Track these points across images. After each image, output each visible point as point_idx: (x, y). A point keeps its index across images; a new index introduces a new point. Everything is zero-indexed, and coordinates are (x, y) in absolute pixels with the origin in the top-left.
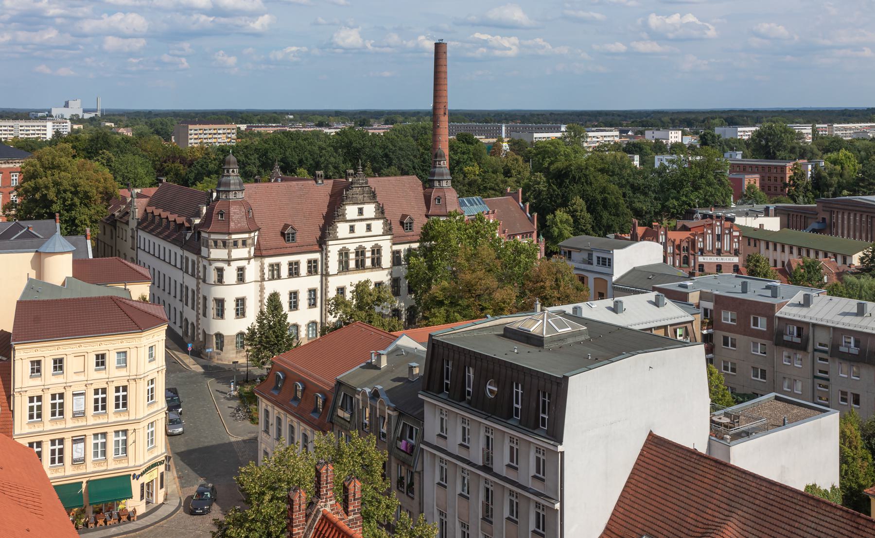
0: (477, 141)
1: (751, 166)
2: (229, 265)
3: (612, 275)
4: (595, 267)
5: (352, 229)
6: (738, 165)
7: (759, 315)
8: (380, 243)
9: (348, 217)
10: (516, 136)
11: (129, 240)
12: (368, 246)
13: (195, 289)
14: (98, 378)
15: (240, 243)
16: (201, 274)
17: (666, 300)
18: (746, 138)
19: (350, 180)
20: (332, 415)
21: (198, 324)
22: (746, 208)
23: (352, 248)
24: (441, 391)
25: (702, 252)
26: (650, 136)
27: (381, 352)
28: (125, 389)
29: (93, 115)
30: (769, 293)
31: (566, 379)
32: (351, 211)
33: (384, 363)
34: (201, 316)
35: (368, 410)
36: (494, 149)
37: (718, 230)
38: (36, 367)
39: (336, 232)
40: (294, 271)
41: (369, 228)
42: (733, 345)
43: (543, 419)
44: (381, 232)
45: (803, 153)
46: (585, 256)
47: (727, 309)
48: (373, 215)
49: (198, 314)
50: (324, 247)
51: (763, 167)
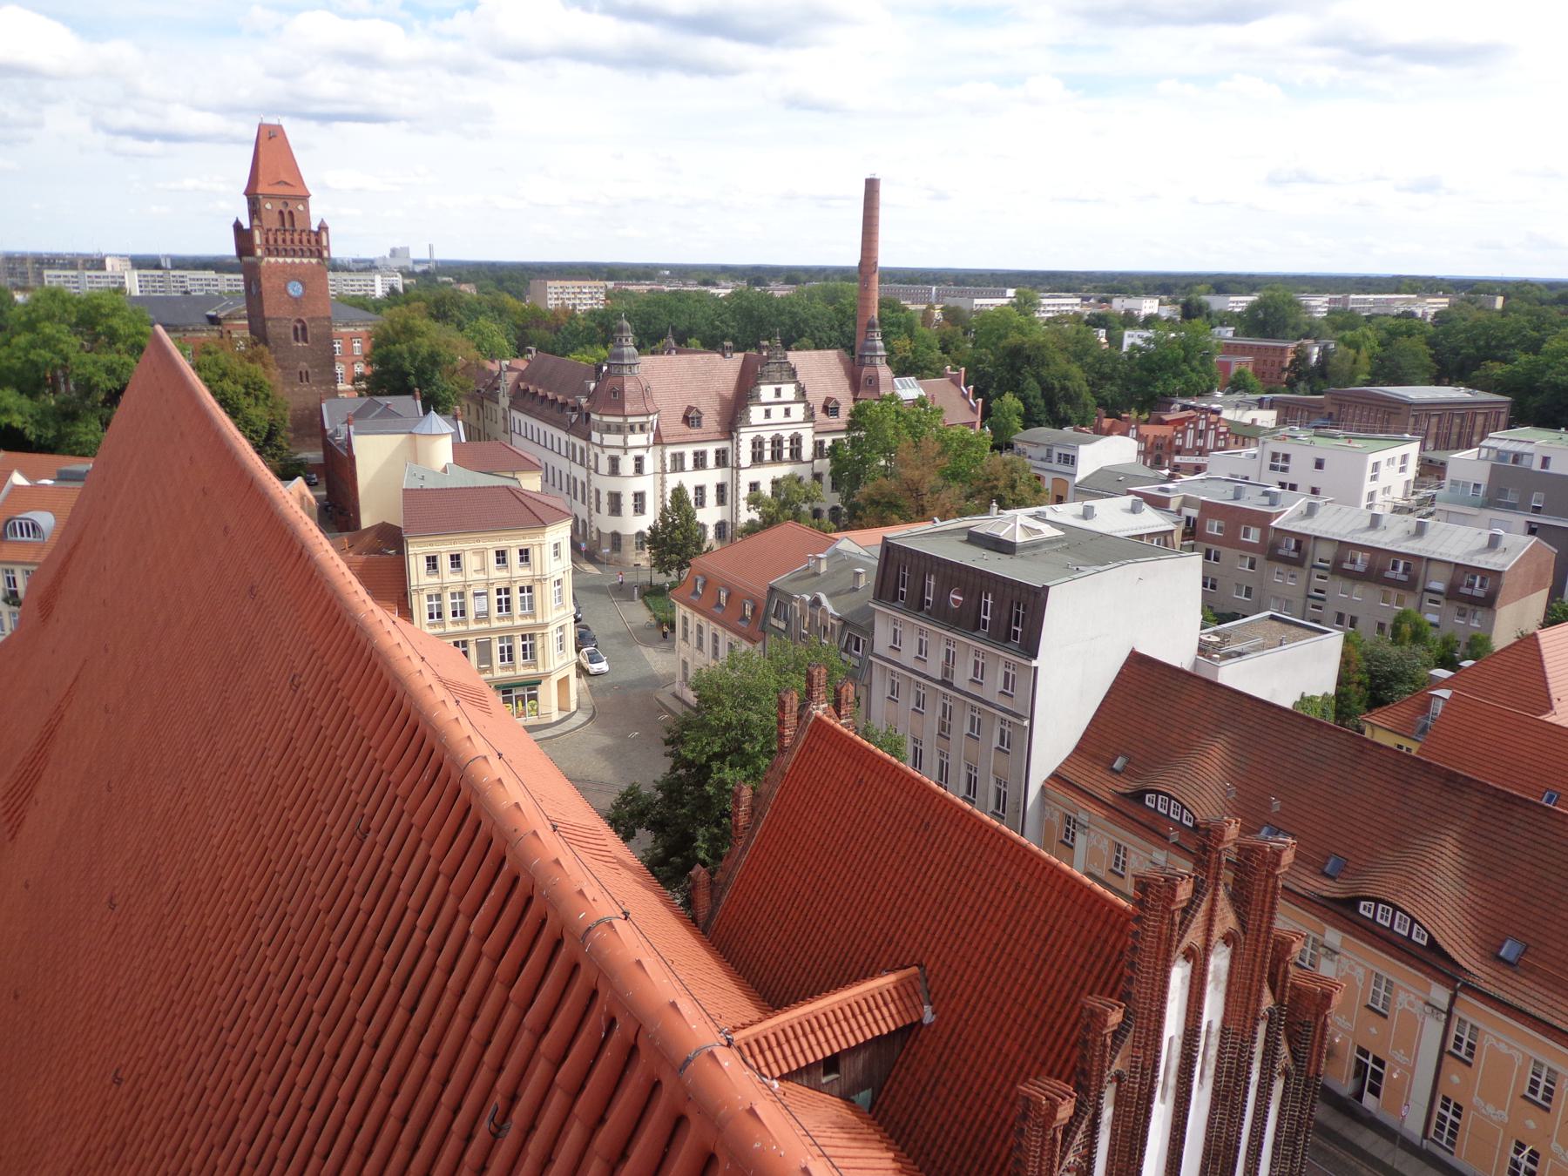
0: (904, 309)
1: (1244, 346)
2: (626, 453)
3: (1074, 475)
4: (1055, 466)
5: (768, 414)
6: (1228, 345)
7: (1253, 525)
8: (799, 431)
9: (764, 399)
10: (951, 302)
11: (501, 421)
12: (786, 435)
13: (585, 480)
14: (497, 575)
15: (637, 427)
16: (592, 464)
17: (1145, 506)
18: (1237, 310)
19: (765, 354)
20: (764, 623)
21: (590, 521)
22: (1237, 397)
23: (767, 436)
24: (895, 600)
25: (1178, 452)
26: (1119, 305)
27: (821, 556)
28: (530, 589)
29: (425, 267)
30: (1266, 500)
31: (1046, 589)
32: (767, 392)
33: (823, 568)
34: (594, 511)
35: (807, 619)
36: (927, 316)
37: (1202, 425)
38: (432, 562)
39: (748, 417)
40: (700, 460)
41: (787, 412)
42: (1216, 559)
43: (1016, 632)
44: (801, 418)
45: (1312, 331)
46: (1043, 452)
47: (1214, 517)
48: (792, 397)
49: (590, 509)
50: (735, 434)
51: (1259, 347)
